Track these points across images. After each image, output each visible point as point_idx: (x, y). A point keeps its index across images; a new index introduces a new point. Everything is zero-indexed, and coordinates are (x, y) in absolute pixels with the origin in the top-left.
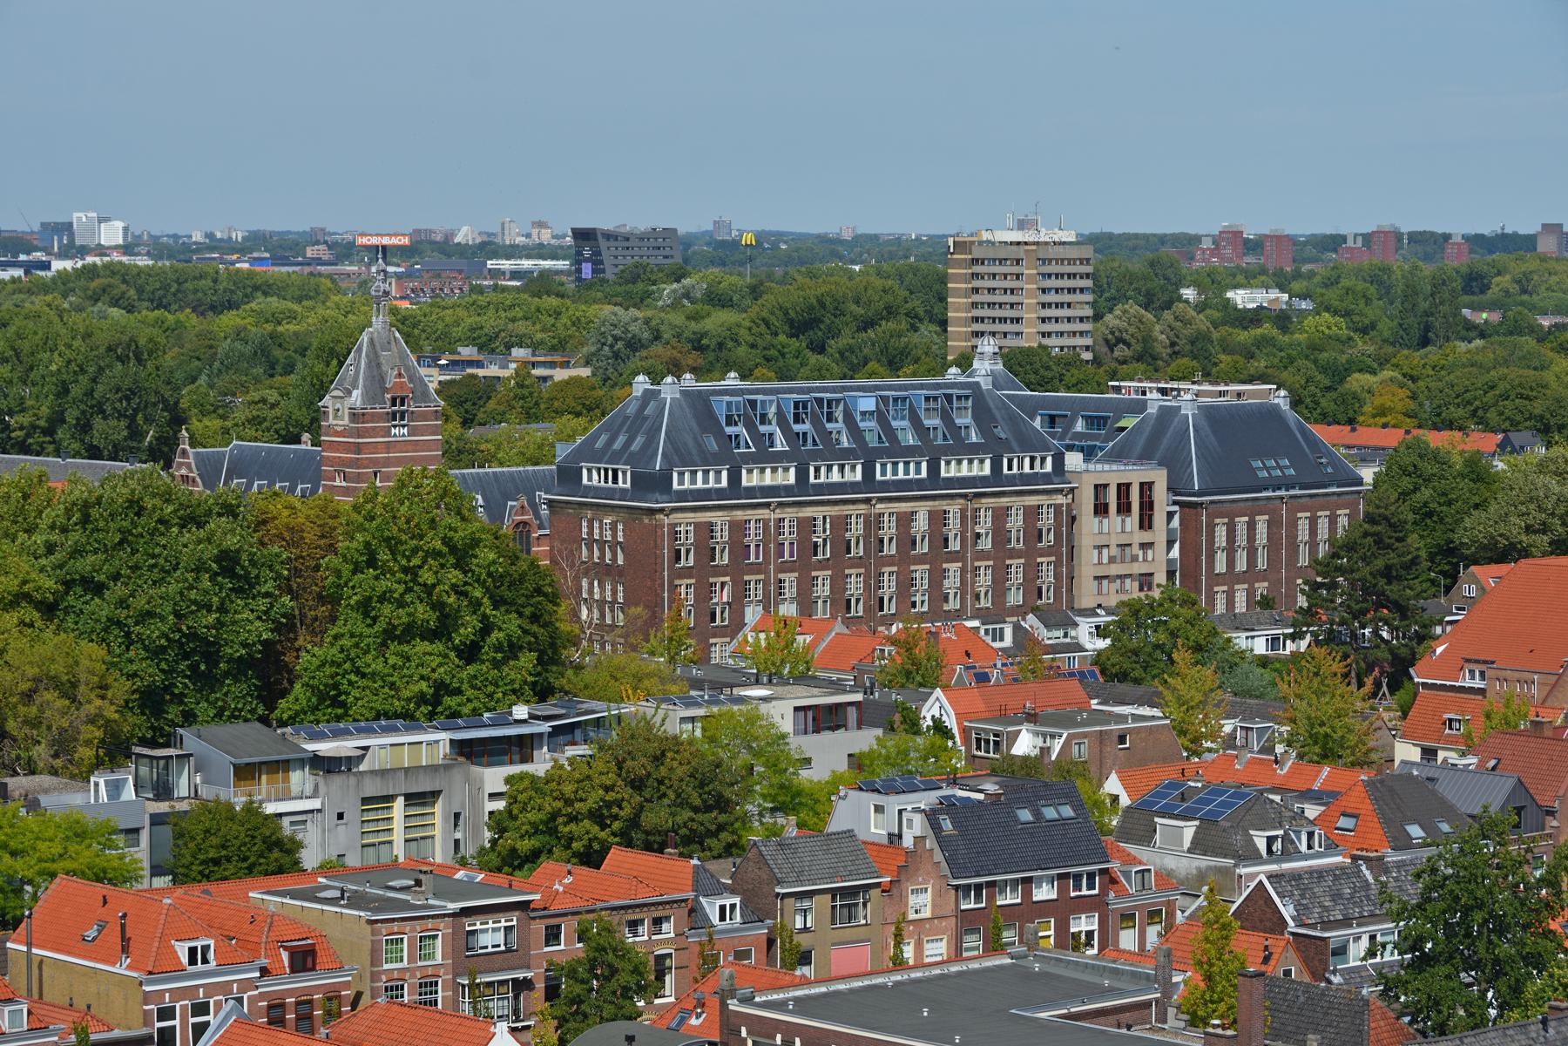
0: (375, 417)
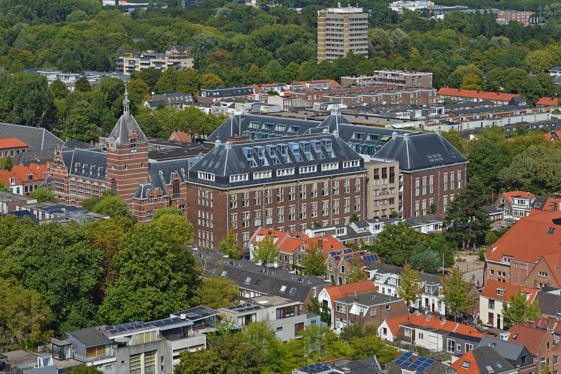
0: (125, 147)
